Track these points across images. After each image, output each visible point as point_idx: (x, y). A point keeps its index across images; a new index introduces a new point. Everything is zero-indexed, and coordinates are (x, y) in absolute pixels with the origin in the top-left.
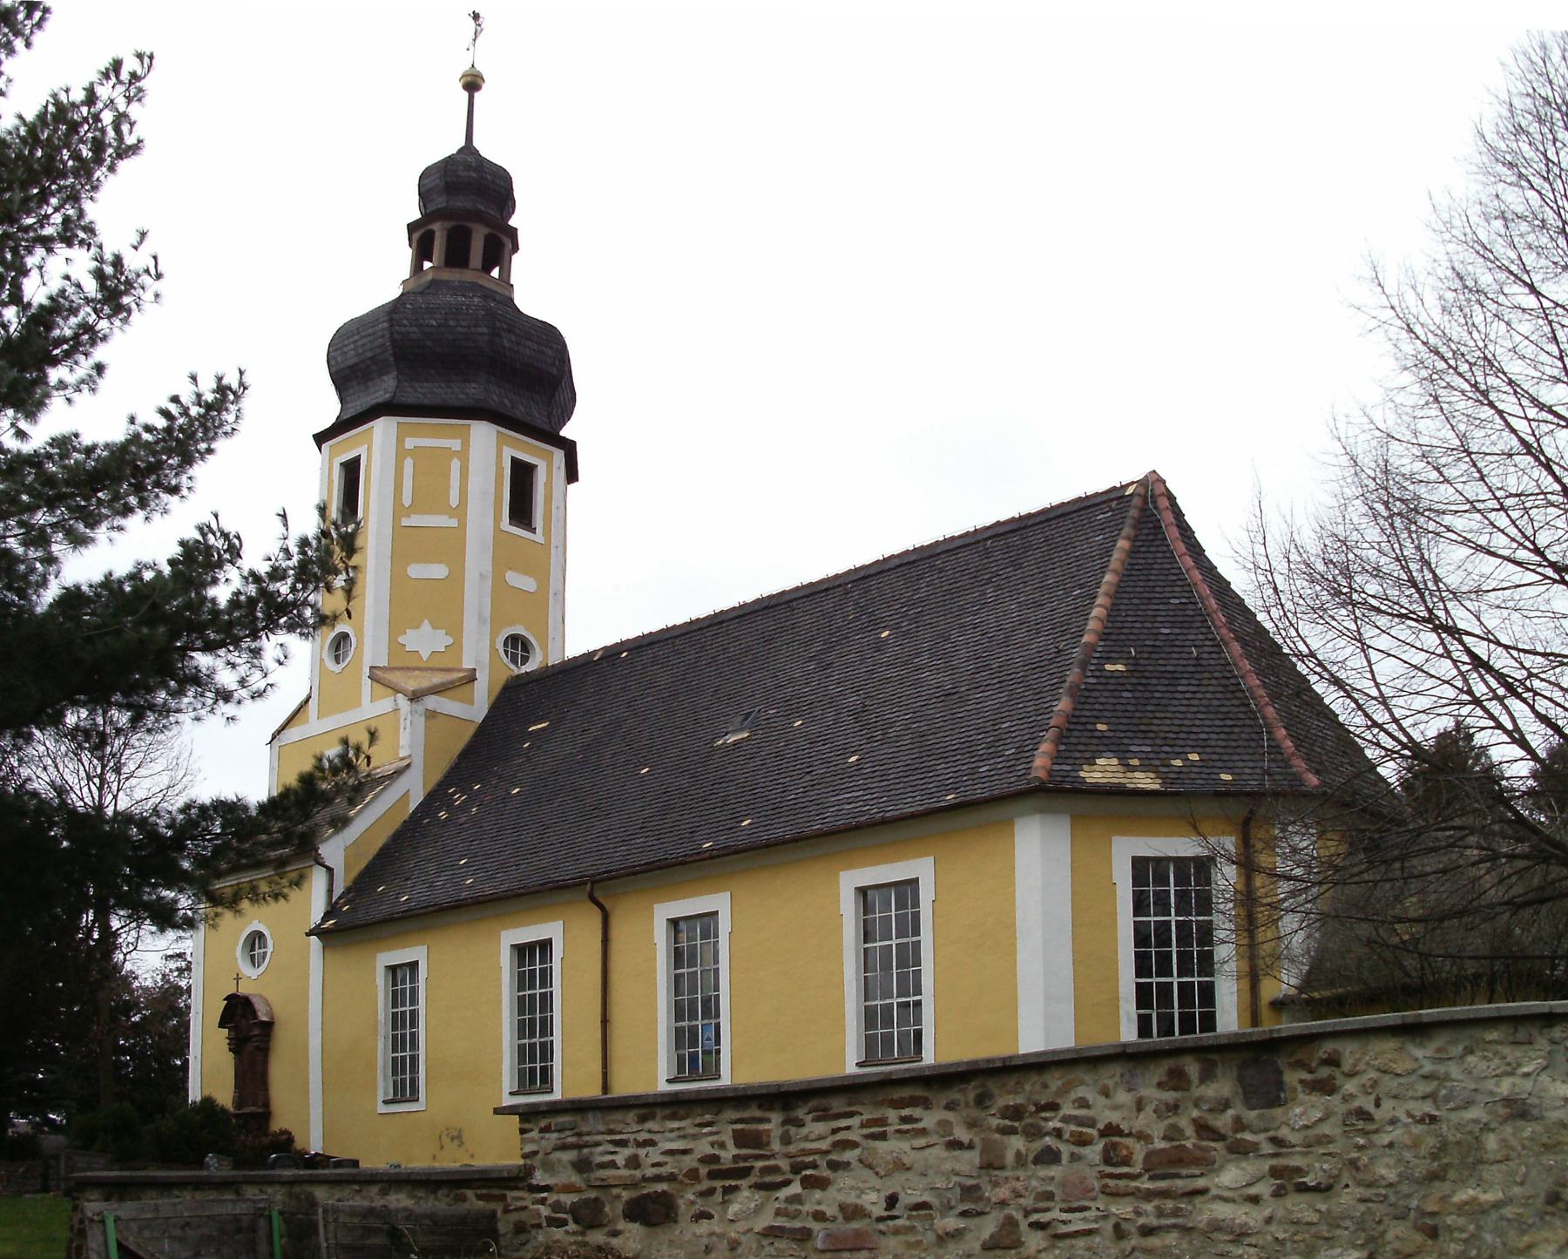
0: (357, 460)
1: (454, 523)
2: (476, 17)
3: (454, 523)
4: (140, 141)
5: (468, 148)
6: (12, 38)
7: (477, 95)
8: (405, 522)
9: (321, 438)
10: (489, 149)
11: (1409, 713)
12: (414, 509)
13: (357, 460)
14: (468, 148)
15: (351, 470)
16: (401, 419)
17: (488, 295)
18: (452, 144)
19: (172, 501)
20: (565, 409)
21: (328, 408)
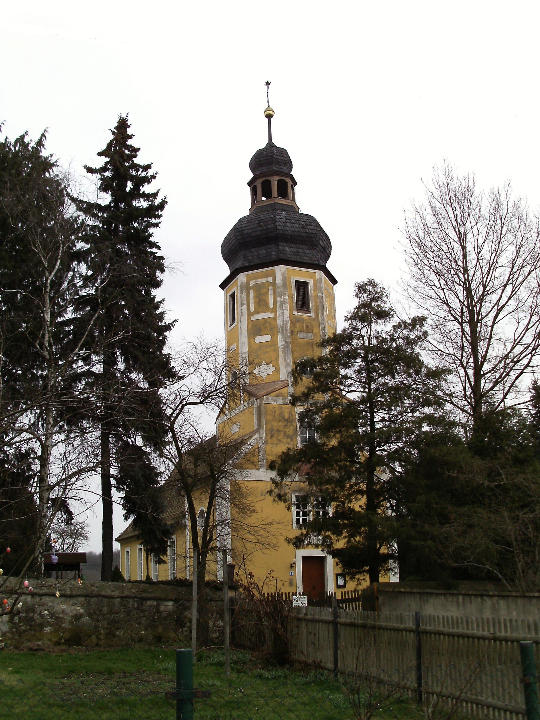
0: (234, 293)
1: (272, 315)
2: (268, 84)
3: (272, 315)
4: (361, 288)
5: (271, 145)
6: (149, 203)
7: (272, 119)
8: (252, 318)
9: (223, 286)
10: (278, 143)
11: (502, 236)
12: (256, 312)
13: (234, 293)
14: (271, 145)
15: (233, 296)
16: (247, 273)
17: (285, 208)
18: (262, 144)
19: (87, 529)
20: (326, 252)
21: (225, 271)
